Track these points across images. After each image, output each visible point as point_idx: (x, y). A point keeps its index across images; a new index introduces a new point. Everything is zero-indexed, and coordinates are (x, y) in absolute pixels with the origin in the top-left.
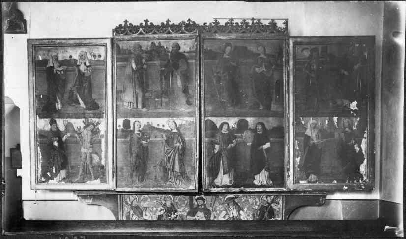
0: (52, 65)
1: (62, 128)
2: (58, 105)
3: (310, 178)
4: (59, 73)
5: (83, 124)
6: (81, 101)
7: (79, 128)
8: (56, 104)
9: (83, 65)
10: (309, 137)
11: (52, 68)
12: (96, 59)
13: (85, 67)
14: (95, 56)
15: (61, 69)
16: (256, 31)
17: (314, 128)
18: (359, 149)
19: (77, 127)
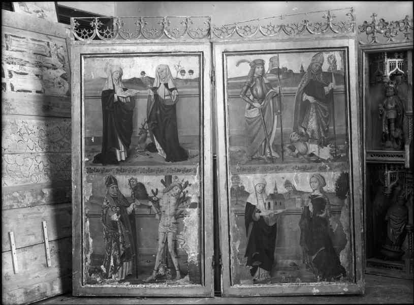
0: (112, 88)
1: (127, 192)
3: (257, 274)
4: (122, 100)
5: (162, 185)
7: (155, 191)
8: (118, 151)
9: (162, 86)
10: (255, 206)
11: (112, 92)
12: (185, 77)
13: (166, 90)
14: (183, 72)
15: (128, 93)
16: (93, 36)
18: (337, 225)
19: (152, 191)
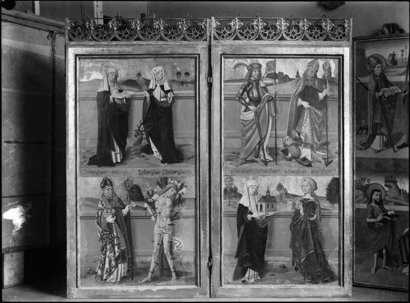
2: (116, 154)
3: (247, 275)
6: (154, 149)
9: (158, 88)
17: (256, 193)
